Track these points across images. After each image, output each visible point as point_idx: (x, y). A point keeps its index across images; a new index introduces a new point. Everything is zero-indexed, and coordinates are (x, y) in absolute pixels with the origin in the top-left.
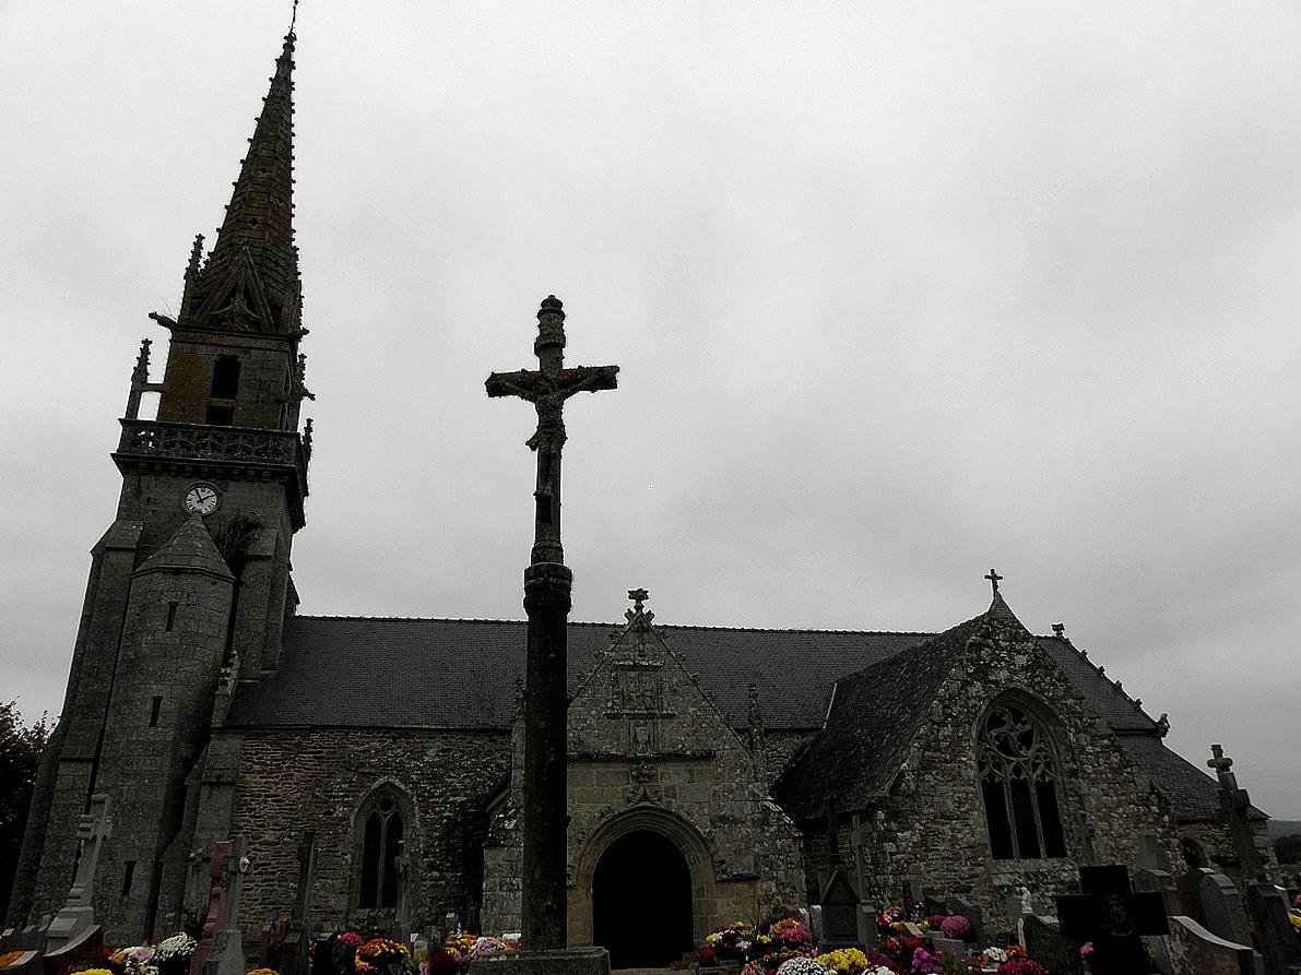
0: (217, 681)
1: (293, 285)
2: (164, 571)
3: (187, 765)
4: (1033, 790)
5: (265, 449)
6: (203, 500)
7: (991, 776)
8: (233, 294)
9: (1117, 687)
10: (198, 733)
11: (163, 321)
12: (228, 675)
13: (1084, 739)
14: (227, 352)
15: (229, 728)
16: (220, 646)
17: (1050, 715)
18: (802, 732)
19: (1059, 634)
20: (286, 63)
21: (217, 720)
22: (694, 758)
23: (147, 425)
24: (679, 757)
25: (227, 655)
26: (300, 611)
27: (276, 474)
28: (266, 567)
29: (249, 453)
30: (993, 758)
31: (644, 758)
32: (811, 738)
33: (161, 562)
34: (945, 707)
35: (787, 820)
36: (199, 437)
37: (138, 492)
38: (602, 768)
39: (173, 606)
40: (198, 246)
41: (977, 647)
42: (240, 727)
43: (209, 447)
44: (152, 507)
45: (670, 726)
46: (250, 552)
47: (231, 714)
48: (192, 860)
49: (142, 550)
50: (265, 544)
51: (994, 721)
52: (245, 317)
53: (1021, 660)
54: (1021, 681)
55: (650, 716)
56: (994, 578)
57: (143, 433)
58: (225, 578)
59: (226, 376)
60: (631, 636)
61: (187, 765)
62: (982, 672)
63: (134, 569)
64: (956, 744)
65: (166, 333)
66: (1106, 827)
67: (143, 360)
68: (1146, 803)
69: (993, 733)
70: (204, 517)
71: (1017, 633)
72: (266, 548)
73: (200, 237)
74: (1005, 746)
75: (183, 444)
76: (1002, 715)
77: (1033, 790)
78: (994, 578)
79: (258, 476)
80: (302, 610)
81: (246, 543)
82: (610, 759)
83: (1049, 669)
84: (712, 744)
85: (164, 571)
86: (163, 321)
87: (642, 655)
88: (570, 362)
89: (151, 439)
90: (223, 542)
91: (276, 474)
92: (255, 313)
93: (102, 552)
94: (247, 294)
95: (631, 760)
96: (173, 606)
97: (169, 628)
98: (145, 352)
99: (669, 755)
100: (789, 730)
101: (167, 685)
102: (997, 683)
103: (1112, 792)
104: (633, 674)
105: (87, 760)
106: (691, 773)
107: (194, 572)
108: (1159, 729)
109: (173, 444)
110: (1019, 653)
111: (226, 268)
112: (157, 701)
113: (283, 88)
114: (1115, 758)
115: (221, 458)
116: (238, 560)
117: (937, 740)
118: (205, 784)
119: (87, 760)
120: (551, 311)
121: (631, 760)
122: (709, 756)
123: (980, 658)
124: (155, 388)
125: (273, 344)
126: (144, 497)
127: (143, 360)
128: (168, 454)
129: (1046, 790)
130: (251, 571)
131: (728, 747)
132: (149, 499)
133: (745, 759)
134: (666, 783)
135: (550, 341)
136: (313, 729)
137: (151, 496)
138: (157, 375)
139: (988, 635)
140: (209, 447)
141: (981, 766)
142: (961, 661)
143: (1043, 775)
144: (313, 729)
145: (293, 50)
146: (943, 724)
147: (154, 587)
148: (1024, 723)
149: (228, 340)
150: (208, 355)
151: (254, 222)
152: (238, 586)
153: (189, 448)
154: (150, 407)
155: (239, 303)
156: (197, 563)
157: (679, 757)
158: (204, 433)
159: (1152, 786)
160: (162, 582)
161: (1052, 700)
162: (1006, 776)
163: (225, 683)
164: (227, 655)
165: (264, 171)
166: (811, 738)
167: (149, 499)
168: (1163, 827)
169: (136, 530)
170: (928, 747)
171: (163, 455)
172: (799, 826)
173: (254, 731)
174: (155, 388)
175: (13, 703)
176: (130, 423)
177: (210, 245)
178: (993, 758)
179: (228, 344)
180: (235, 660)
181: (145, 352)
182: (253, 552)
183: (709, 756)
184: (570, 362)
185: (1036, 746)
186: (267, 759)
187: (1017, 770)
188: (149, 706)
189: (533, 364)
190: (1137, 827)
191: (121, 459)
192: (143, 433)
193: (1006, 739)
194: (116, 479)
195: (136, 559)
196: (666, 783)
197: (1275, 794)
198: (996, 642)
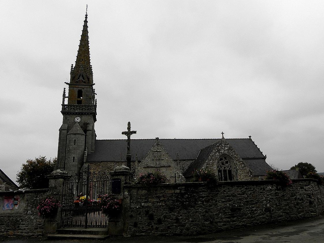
0: (84, 154)
1: (91, 73)
2: (73, 134)
3: (80, 168)
4: (227, 171)
5: (89, 109)
6: (78, 119)
7: (220, 169)
8: (80, 76)
9: (259, 149)
10: (82, 163)
11: (67, 84)
12: (86, 152)
13: (237, 162)
14: (80, 89)
15: (86, 162)
16: (84, 147)
17: (231, 158)
18: (192, 160)
19: (250, 138)
20: (85, 27)
21: (85, 161)
22: (167, 167)
23: (66, 105)
24: (164, 167)
25: (85, 149)
26: (97, 139)
27: (91, 114)
28: (91, 132)
29: (86, 110)
30: (220, 166)
31: (158, 167)
32: (194, 161)
33: (72, 132)
34: (211, 157)
35: (183, 177)
36: (76, 107)
37: (66, 118)
38: (151, 169)
39: (75, 140)
40: (72, 66)
41: (218, 146)
42: (89, 162)
43: (78, 109)
44: (69, 121)
45: (163, 161)
46: (88, 129)
47: (87, 160)
48: (83, 185)
49: (68, 129)
50: (90, 128)
51: (221, 159)
52: (82, 81)
53: (226, 148)
54: (226, 152)
55: (159, 160)
56: (223, 133)
57: (66, 107)
58: (84, 135)
59: (80, 93)
60: (156, 146)
61: (80, 168)
62: (219, 151)
63: (67, 133)
64: (213, 164)
65: (68, 86)
66: (240, 177)
67: (64, 92)
68: (248, 173)
69: (221, 161)
70: (79, 122)
71: (226, 143)
72: (90, 128)
73: (72, 65)
74: (223, 164)
75: (73, 109)
76: (223, 158)
77: (227, 171)
78: (223, 133)
79: (88, 114)
80: (97, 139)
81: (87, 127)
82: (152, 167)
83: (232, 150)
84: (170, 164)
85: (73, 134)
86: (67, 84)
87: (158, 149)
88: (131, 130)
89: (67, 108)
90: (82, 127)
91: (91, 114)
92: (84, 80)
93: (61, 130)
94: (82, 76)
95: (156, 167)
96: (75, 140)
97: (75, 145)
98: (65, 90)
99: (163, 166)
100: (189, 160)
101: (76, 154)
102: (221, 153)
103: (241, 171)
104: (156, 152)
105: (63, 168)
106: (166, 169)
107: (78, 134)
108: (264, 158)
109: (71, 109)
110: (226, 147)
111: (78, 71)
112: (74, 158)
113: (86, 28)
114: (243, 165)
115: (81, 111)
116: (85, 131)
117: (209, 163)
118: (84, 172)
119: (63, 168)
120: (129, 123)
121: (156, 167)
122: (170, 166)
123: (218, 148)
124: (67, 97)
125: (88, 87)
126: (67, 119)
127: (64, 92)
128: (71, 111)
129: (230, 171)
130: (88, 132)
131: (173, 164)
132: (68, 120)
133: (176, 167)
134: (162, 171)
135: (129, 128)
136: (101, 162)
137: (69, 119)
138: (67, 95)
139: (221, 144)
140: (78, 109)
141: (218, 167)
142: (215, 149)
143: (229, 169)
144: (101, 162)
145: (87, 18)
146: (211, 160)
147: (71, 137)
148: (227, 160)
149: (80, 86)
150: (76, 90)
151: (82, 60)
152: (86, 136)
153: (75, 109)
154: (66, 103)
155: (81, 78)
156: (78, 132)
157: (164, 167)
158: (77, 106)
159: (249, 170)
160: (73, 136)
161: (232, 155)
162: (222, 169)
163: (85, 154)
164: (85, 149)
165: (83, 48)
166: (194, 161)
167: (68, 120)
168: (251, 177)
169: (66, 126)
170: (208, 164)
171: (70, 111)
172: (185, 178)
173: (91, 162)
174: (67, 97)
175: (45, 156)
176: (63, 105)
177: (74, 66)
178: (220, 166)
179: (80, 87)
180: (87, 149)
181: (65, 90)
182: (87, 129)
183: (170, 166)
184: (131, 130)
185: (228, 163)
186: (94, 167)
187: (225, 168)
188: (73, 158)
189: (127, 131)
190: (246, 177)
191: (63, 112)
192: (66, 107)
193: (223, 162)
194: (62, 116)
195: (67, 131)
196: (162, 171)
197: (319, 170)
198: (222, 145)
